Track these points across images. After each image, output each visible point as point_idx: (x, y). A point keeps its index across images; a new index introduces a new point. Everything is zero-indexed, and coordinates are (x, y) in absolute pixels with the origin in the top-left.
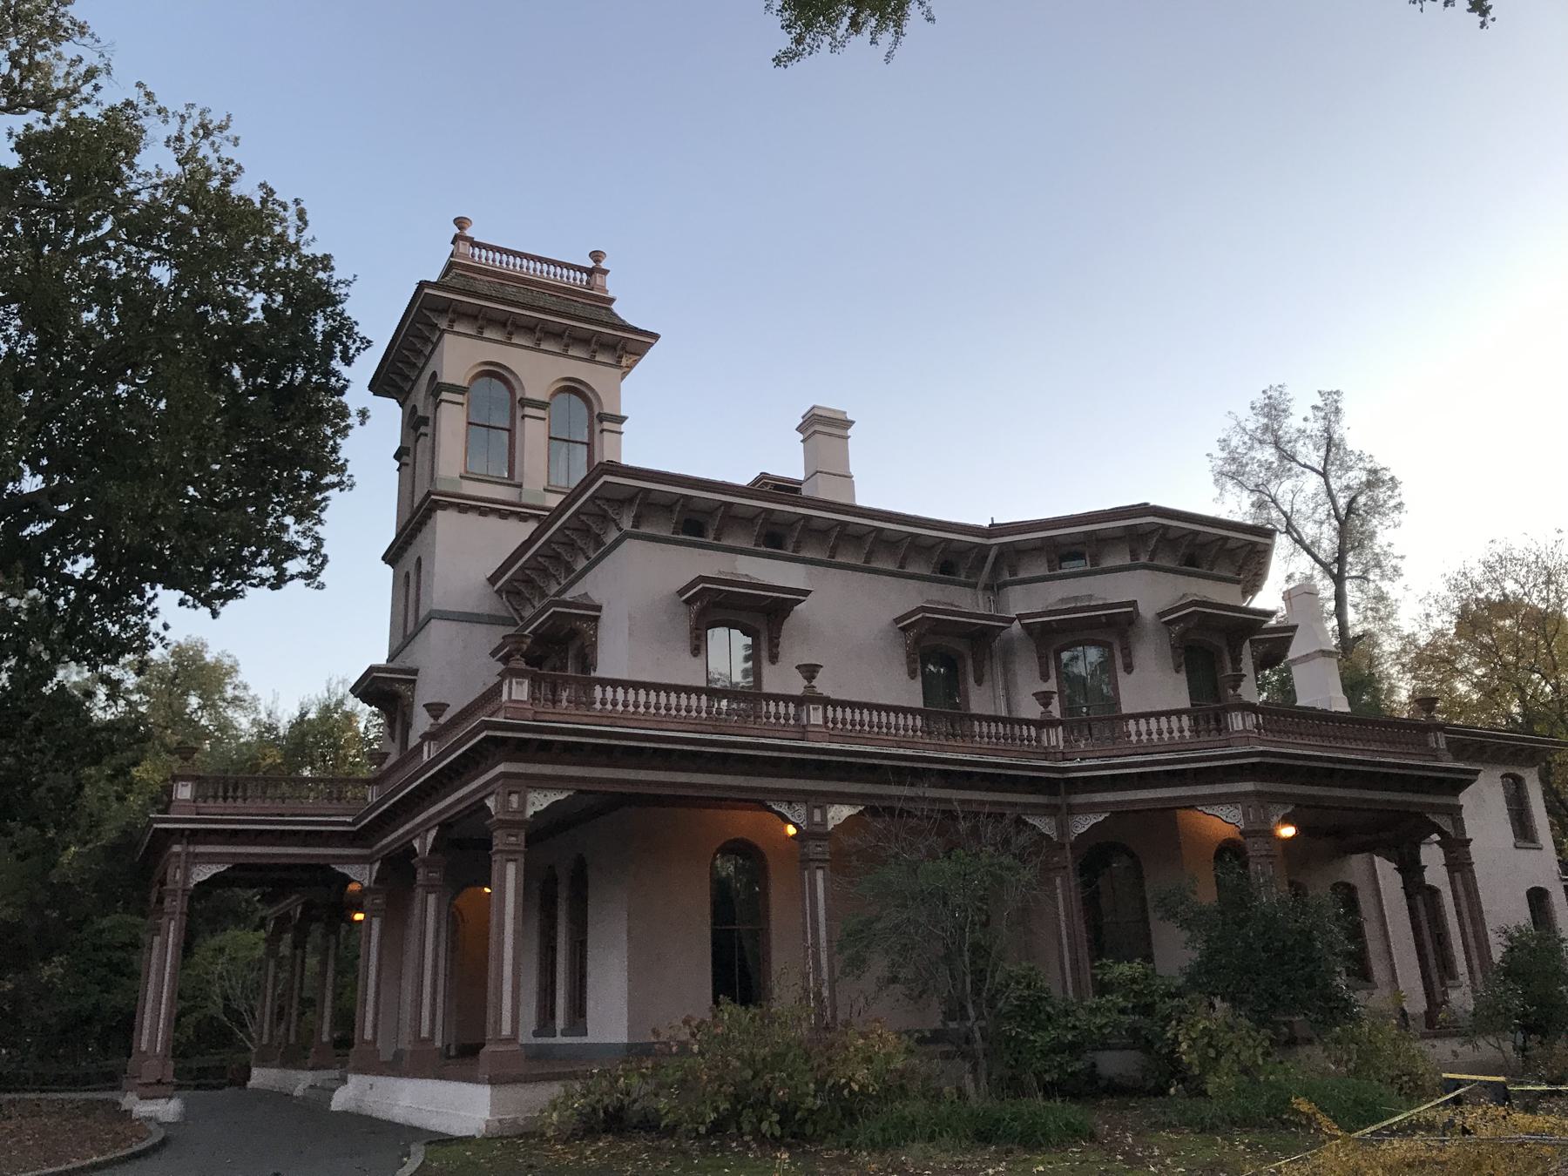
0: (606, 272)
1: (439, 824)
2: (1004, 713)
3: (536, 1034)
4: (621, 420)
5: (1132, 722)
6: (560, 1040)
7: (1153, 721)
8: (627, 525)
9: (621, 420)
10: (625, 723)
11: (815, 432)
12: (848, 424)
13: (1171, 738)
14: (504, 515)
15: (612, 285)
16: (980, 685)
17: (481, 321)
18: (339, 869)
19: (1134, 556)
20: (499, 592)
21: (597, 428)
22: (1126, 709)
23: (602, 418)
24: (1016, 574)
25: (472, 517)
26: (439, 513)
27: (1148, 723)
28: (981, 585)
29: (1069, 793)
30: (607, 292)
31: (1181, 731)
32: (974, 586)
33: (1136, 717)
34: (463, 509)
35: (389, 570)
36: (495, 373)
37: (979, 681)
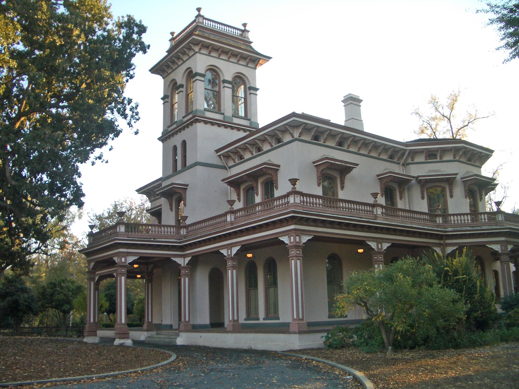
0: (248, 31)
1: (392, 243)
2: (408, 209)
3: (245, 320)
4: (257, 89)
5: (452, 217)
6: (261, 321)
7: (459, 217)
8: (296, 135)
9: (257, 89)
10: (324, 212)
11: (351, 103)
12: (361, 101)
13: (461, 223)
14: (219, 125)
15: (251, 37)
16: (423, 199)
17: (211, 49)
18: (174, 259)
19: (454, 157)
20: (219, 156)
21: (248, 92)
22: (450, 212)
23: (251, 88)
24: (413, 161)
25: (209, 126)
26: (198, 124)
27: (461, 217)
28: (401, 164)
29: (446, 239)
30: (249, 39)
31: (468, 220)
32: (399, 164)
33: (453, 215)
34: (206, 123)
35: (161, 143)
36: (213, 69)
37: (401, 198)
